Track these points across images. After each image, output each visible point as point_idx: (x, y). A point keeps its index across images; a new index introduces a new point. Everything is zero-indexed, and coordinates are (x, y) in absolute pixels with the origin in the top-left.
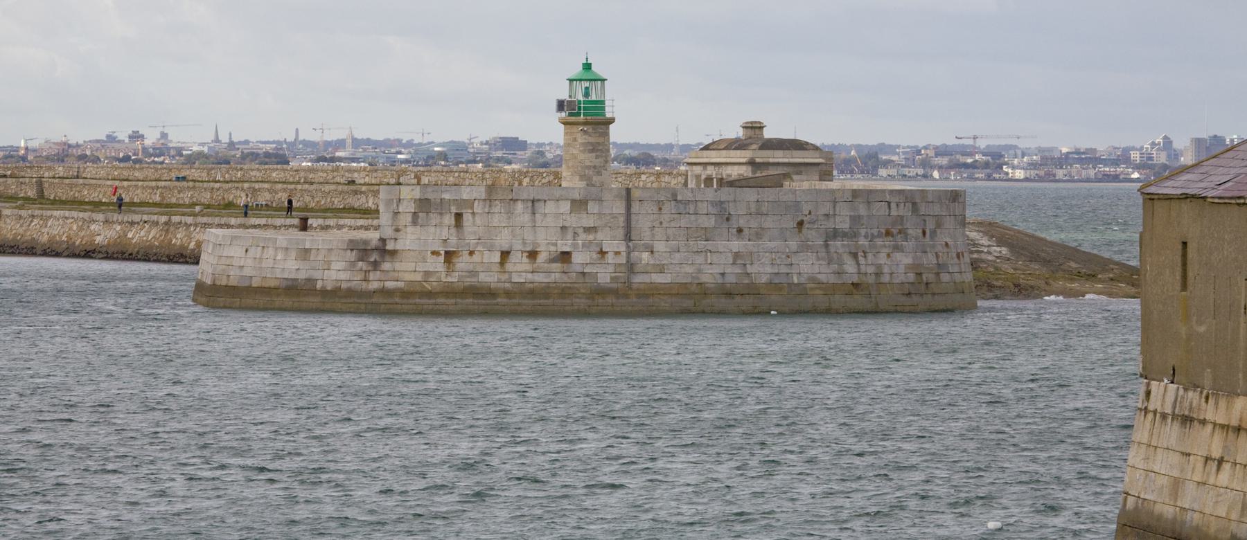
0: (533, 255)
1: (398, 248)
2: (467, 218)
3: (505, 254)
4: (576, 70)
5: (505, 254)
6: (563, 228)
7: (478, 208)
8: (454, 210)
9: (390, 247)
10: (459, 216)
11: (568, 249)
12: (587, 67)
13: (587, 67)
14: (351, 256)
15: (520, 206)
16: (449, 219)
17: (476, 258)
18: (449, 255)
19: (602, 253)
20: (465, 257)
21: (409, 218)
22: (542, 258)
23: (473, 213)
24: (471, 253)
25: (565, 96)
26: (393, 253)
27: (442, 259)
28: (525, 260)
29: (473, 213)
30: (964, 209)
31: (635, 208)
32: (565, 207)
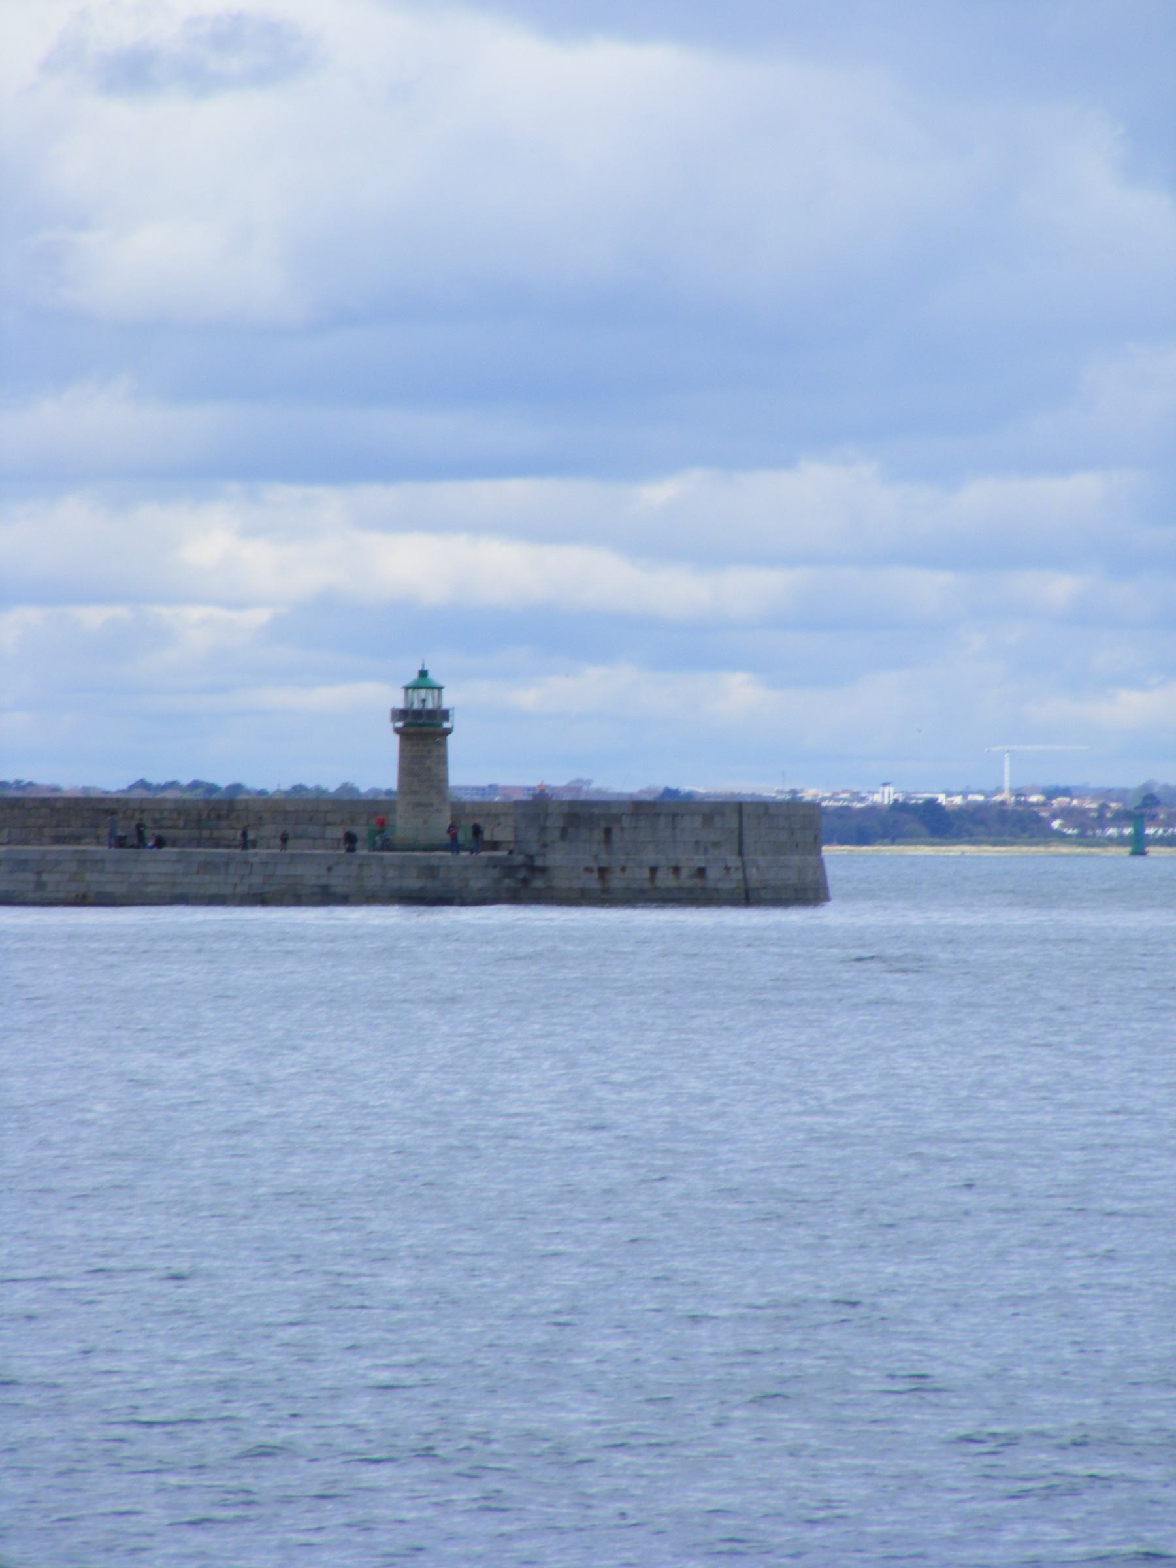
0: (676, 870)
1: (548, 863)
2: (616, 835)
3: (654, 870)
4: (413, 676)
5: (654, 870)
6: (697, 843)
7: (626, 822)
8: (603, 824)
9: (539, 862)
10: (608, 831)
11: (702, 865)
12: (423, 674)
13: (423, 674)
14: (495, 873)
15: (662, 820)
16: (598, 835)
17: (628, 874)
18: (603, 871)
19: (727, 869)
20: (618, 873)
21: (556, 834)
22: (684, 873)
23: (622, 829)
24: (623, 869)
25: (400, 705)
26: (544, 870)
27: (596, 875)
28: (671, 876)
29: (622, 829)
30: (132, 847)
31: (745, 819)
32: (698, 822)
